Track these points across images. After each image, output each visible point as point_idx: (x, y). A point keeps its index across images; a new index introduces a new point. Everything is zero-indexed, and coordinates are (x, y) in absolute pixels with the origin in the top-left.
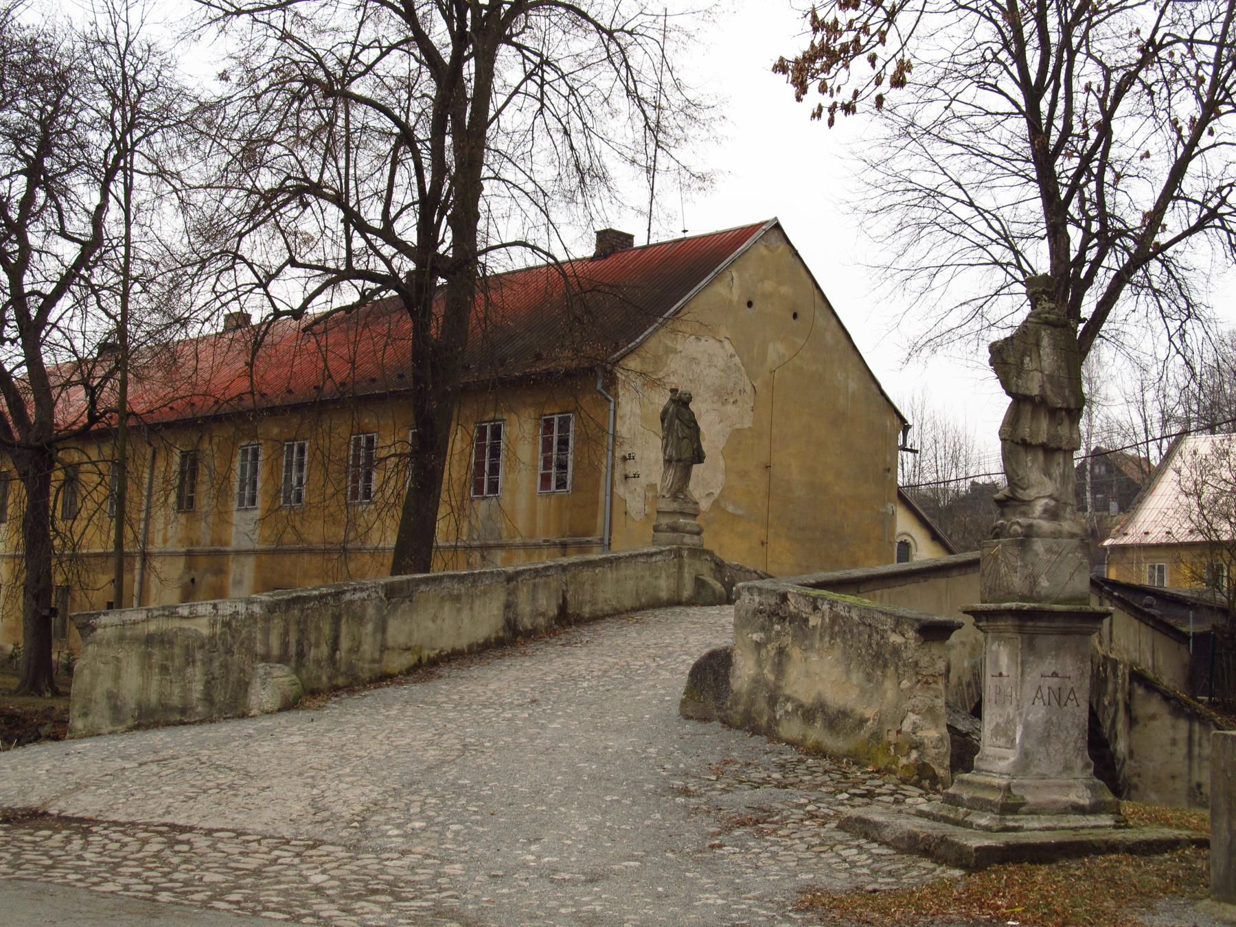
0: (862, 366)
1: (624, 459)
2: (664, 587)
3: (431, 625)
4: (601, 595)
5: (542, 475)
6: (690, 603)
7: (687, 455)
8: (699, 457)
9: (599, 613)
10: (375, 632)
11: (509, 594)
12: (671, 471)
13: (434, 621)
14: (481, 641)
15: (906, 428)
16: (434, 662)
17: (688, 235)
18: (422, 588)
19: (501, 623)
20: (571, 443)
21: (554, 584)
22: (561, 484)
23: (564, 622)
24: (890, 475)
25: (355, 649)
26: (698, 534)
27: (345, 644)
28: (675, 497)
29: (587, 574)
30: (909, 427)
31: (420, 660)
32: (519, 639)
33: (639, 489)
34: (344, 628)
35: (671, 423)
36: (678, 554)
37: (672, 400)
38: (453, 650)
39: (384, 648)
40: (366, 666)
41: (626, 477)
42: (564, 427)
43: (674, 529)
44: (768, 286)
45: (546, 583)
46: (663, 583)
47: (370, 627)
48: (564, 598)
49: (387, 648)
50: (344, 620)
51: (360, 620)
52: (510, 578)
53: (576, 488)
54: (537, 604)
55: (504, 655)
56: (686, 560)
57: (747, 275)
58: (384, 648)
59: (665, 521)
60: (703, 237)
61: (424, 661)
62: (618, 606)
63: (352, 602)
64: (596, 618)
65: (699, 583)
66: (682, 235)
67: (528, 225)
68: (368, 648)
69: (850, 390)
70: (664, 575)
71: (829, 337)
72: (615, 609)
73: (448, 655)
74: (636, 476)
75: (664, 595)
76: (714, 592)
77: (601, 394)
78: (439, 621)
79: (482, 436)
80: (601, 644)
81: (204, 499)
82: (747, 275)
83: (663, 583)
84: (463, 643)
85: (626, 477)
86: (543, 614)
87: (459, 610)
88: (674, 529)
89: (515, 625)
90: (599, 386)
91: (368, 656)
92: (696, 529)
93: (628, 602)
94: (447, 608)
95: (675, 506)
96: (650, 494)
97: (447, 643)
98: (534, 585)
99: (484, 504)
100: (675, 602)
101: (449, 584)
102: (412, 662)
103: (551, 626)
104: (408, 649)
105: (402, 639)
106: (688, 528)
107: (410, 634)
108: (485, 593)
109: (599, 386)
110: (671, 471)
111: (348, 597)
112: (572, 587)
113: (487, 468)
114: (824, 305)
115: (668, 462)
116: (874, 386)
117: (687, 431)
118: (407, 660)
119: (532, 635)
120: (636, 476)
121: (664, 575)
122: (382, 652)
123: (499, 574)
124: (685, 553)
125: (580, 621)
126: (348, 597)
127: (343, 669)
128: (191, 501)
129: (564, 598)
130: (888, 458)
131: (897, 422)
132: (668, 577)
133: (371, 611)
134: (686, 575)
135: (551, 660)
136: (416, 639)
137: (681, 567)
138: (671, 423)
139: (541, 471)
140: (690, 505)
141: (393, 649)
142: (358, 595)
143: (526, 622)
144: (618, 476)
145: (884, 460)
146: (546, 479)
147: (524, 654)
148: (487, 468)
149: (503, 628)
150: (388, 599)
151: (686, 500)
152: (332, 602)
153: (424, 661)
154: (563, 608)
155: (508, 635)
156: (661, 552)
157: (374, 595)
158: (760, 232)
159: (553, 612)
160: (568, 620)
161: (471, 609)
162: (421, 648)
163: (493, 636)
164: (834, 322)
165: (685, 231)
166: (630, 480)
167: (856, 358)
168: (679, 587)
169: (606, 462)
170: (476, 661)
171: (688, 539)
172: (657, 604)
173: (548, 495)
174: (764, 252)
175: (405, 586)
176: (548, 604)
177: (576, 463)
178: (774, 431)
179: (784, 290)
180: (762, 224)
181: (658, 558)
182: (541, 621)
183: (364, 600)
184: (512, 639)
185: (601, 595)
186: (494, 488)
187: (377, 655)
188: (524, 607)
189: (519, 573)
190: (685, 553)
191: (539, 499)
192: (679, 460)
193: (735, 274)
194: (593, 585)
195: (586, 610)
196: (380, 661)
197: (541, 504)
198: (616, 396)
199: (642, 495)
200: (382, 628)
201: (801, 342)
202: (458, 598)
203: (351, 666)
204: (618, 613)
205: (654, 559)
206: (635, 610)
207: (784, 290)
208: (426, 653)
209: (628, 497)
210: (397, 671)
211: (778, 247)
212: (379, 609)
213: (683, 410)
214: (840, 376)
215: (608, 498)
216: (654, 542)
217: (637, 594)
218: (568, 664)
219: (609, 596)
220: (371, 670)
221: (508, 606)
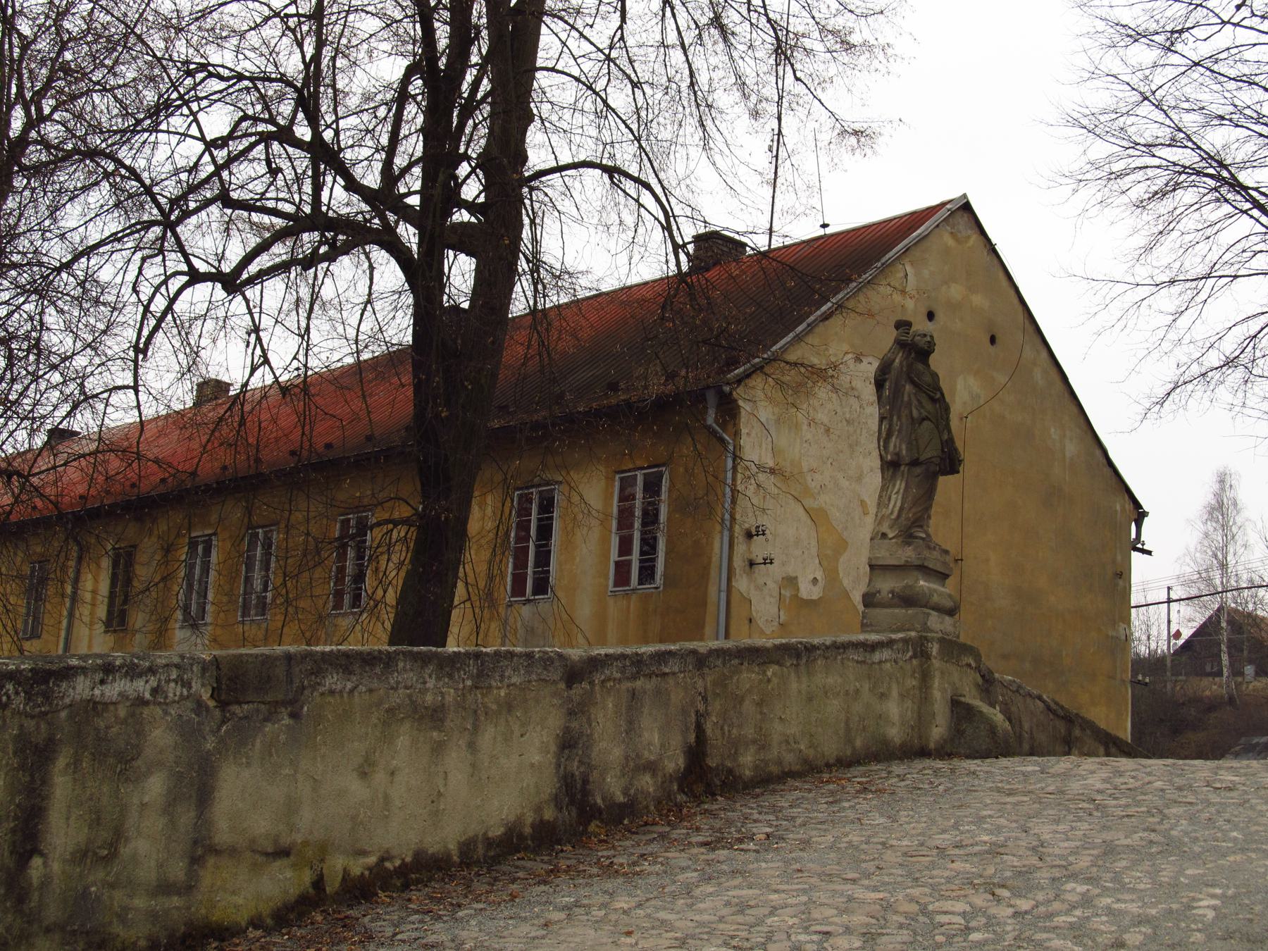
0: (1082, 420)
1: (749, 535)
2: (895, 717)
3: (357, 789)
4: (778, 727)
5: (617, 563)
6: (944, 752)
7: (931, 452)
8: (950, 462)
9: (774, 769)
10: (171, 803)
11: (571, 713)
12: (900, 485)
13: (364, 775)
14: (496, 832)
15: (1139, 515)
16: (361, 890)
17: (829, 231)
18: (333, 680)
19: (549, 785)
20: (663, 517)
21: (677, 697)
22: (647, 572)
23: (699, 788)
24: (1121, 582)
25: (104, 849)
26: (951, 612)
27: (63, 832)
28: (907, 536)
29: (748, 677)
30: (1145, 514)
31: (319, 883)
32: (592, 827)
33: (771, 585)
34: (61, 786)
35: (897, 391)
36: (922, 653)
37: (901, 344)
38: (418, 854)
39: (202, 850)
40: (140, 902)
41: (752, 564)
42: (652, 487)
43: (907, 600)
44: (956, 291)
45: (658, 692)
46: (893, 709)
47: (155, 786)
48: (700, 730)
49: (215, 851)
50: (61, 762)
51: (123, 762)
52: (575, 674)
53: (669, 580)
54: (634, 743)
55: (555, 871)
56: (936, 663)
57: (926, 273)
58: (202, 850)
59: (887, 585)
60: (854, 230)
61: (333, 885)
62: (811, 753)
63: (95, 707)
64: (768, 780)
65: (961, 711)
66: (821, 232)
67: (592, 247)
68: (149, 848)
69: (1068, 455)
70: (895, 693)
71: (1038, 375)
72: (806, 761)
73: (403, 870)
74: (768, 561)
75: (895, 733)
76: (992, 729)
77: (714, 433)
78: (380, 777)
79: (524, 511)
80: (806, 844)
81: (138, 618)
82: (926, 273)
83: (893, 709)
84: (446, 837)
85: (752, 564)
86: (651, 767)
87: (438, 749)
88: (907, 600)
89: (585, 793)
90: (710, 420)
91: (147, 873)
92: (949, 604)
93: (831, 747)
94: (403, 741)
95: (907, 554)
96: (787, 593)
97: (401, 836)
98: (633, 694)
99: (526, 611)
100: (916, 751)
101: (411, 677)
102: (294, 892)
103: (669, 796)
104: (282, 853)
105: (262, 825)
106: (935, 598)
107: (291, 807)
108: (509, 706)
109: (710, 420)
110: (900, 485)
111: (81, 688)
112: (716, 706)
113: (533, 532)
114: (1030, 329)
115: (891, 466)
116: (1098, 452)
117: (929, 406)
118: (282, 882)
119: (624, 817)
120: (768, 561)
121: (895, 693)
122: (195, 861)
123: (547, 661)
124: (934, 649)
125: (733, 785)
126: (81, 688)
127: (53, 913)
128: (123, 615)
129: (700, 730)
130: (1119, 558)
131: (1129, 506)
132: (902, 696)
133: (161, 736)
134: (937, 694)
135: (688, 891)
136: (309, 823)
137: (925, 677)
138: (897, 391)
139: (614, 556)
140: (936, 554)
141: (233, 852)
142: (115, 688)
143: (613, 786)
144: (738, 562)
145: (1114, 561)
146: (622, 571)
147: (609, 870)
148: (533, 532)
149: (556, 799)
150: (223, 705)
151: (928, 543)
152: (19, 702)
153: (333, 885)
154: (696, 753)
155: (569, 815)
156: (890, 643)
157: (173, 690)
158: (943, 214)
159: (675, 762)
160: (706, 783)
161: (472, 746)
162: (323, 850)
163: (529, 818)
164: (1044, 354)
165: (824, 226)
166: (756, 568)
167: (1075, 410)
168: (922, 720)
169: (718, 545)
170: (480, 887)
171: (938, 623)
172: (884, 753)
173: (627, 595)
174: (950, 242)
175: (280, 671)
176: (662, 742)
177: (670, 551)
178: (966, 506)
179: (978, 300)
180: (943, 205)
181: (886, 654)
182: (647, 783)
183: (140, 702)
184: (575, 828)
185: (778, 727)
186: (542, 586)
187: (177, 870)
188: (608, 749)
189: (595, 663)
190: (934, 649)
191: (611, 602)
192: (915, 463)
193: (909, 268)
194: (759, 704)
195: (747, 761)
196: (188, 888)
197: (614, 608)
198: (737, 434)
199: (776, 594)
200: (198, 787)
201: (1002, 379)
202: (434, 716)
203: (81, 901)
204: (810, 770)
205: (877, 656)
206: (844, 763)
207: (978, 300)
208: (338, 865)
209: (754, 596)
210: (242, 918)
211: (969, 237)
212: (188, 733)
213: (920, 367)
214: (1054, 433)
215: (724, 595)
216: (864, 627)
217: (848, 729)
218: (742, 907)
219: (793, 730)
220: (153, 916)
221: (568, 743)
